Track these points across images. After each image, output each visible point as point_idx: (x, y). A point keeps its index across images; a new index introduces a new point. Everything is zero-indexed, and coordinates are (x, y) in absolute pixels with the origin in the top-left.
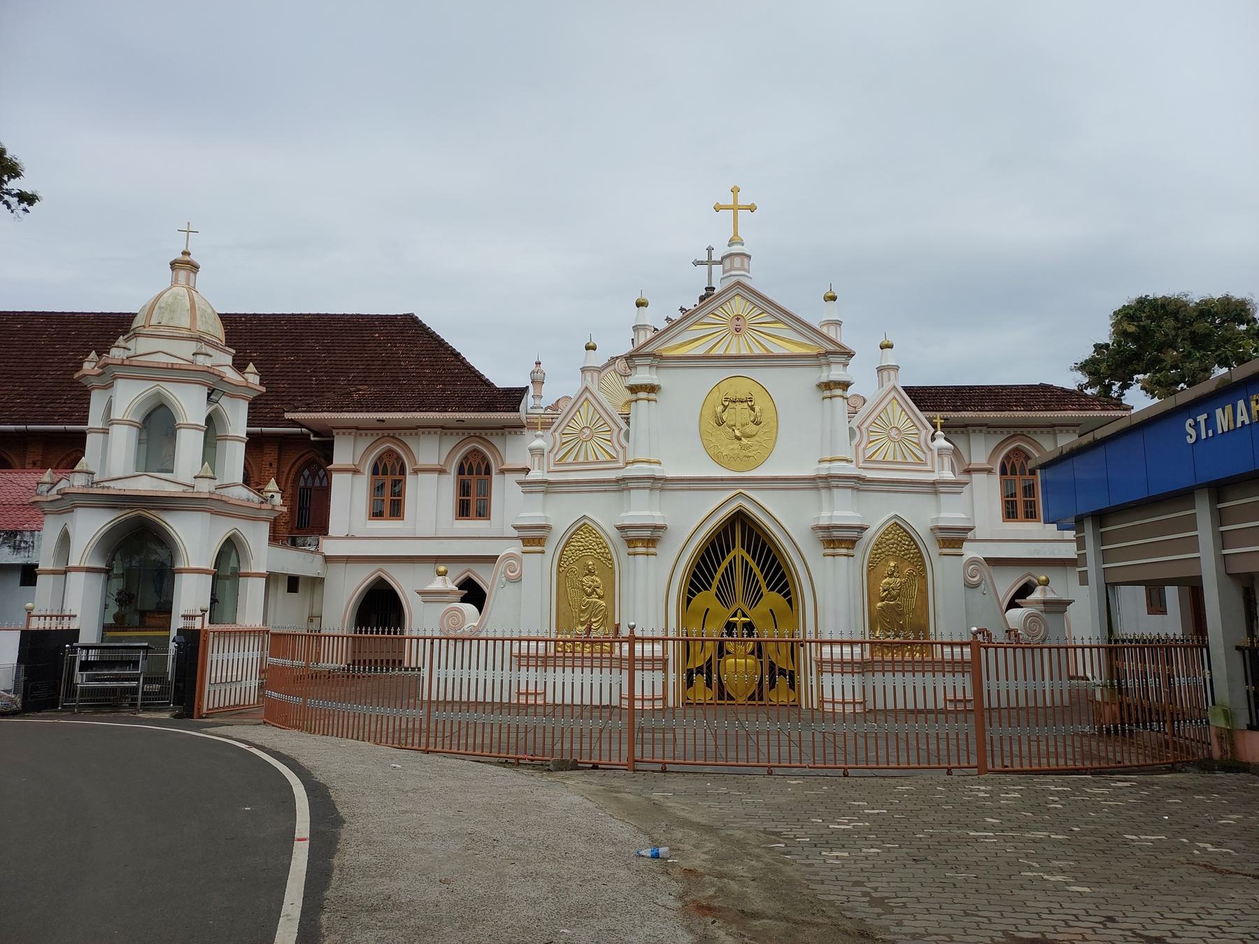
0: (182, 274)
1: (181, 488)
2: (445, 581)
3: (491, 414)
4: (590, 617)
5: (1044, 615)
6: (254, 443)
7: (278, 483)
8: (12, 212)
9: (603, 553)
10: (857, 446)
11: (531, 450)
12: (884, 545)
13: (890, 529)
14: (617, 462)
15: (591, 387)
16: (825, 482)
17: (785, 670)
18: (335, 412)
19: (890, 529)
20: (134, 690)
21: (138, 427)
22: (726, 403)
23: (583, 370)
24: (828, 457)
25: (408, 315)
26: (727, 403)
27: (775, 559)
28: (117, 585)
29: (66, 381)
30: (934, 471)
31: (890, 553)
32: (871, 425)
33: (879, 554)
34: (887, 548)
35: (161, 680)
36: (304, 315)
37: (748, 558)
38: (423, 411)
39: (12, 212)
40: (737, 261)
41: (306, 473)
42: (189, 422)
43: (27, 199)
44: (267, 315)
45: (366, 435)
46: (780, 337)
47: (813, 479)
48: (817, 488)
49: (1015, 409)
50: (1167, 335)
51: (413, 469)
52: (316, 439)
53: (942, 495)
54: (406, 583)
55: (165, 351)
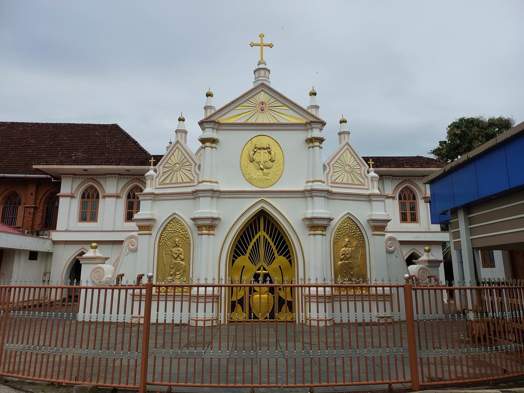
2: (95, 252)
4: (176, 272)
5: (428, 268)
9: (184, 234)
10: (328, 174)
12: (342, 229)
13: (345, 221)
14: (194, 182)
15: (180, 141)
18: (60, 165)
19: (345, 221)
22: (255, 150)
24: (311, 180)
25: (114, 124)
27: (282, 237)
30: (369, 189)
31: (345, 234)
32: (335, 163)
33: (339, 234)
34: (344, 231)
36: (62, 124)
37: (267, 237)
38: (107, 165)
40: (262, 73)
44: (43, 123)
46: (285, 114)
49: (406, 166)
50: (474, 134)
51: (103, 196)
52: (55, 181)
53: (373, 202)
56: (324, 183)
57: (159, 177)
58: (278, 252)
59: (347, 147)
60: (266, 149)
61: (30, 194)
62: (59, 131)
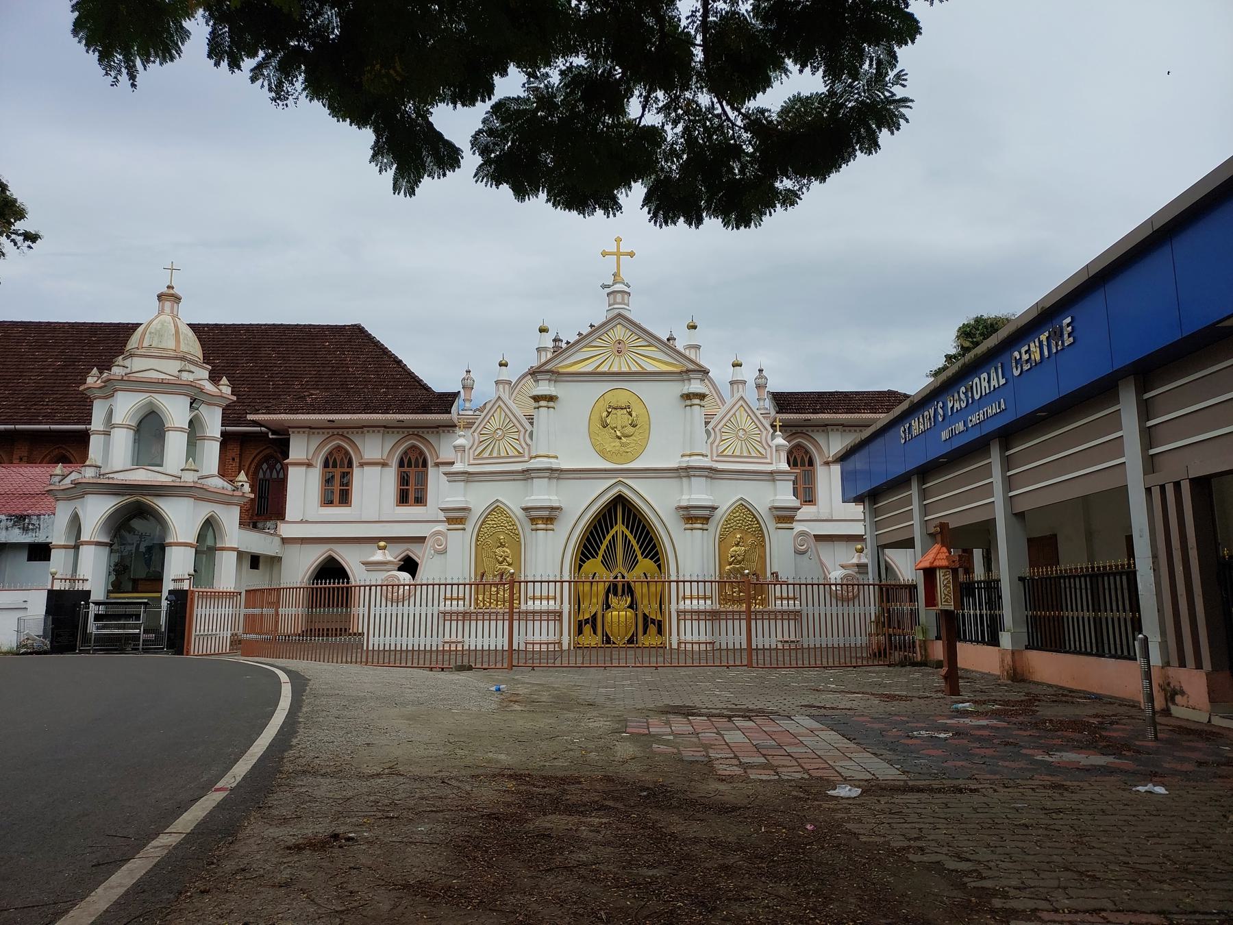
0: (168, 305)
1: (170, 479)
2: (384, 554)
3: (427, 415)
6: (227, 439)
7: (247, 475)
8: (18, 248)
10: (712, 443)
11: (455, 447)
13: (737, 509)
14: (524, 456)
15: (502, 396)
16: (685, 472)
17: (654, 620)
18: (291, 414)
19: (737, 509)
20: (136, 637)
21: (134, 430)
23: (497, 383)
24: (688, 453)
25: (356, 325)
26: (610, 410)
27: (648, 533)
28: (116, 558)
29: (46, 385)
30: (772, 464)
35: (156, 630)
37: (628, 533)
38: (368, 413)
39: (18, 248)
41: (265, 466)
42: (176, 426)
43: (31, 237)
45: (318, 433)
47: (677, 470)
48: (680, 477)
51: (359, 463)
52: (274, 437)
53: (777, 482)
54: (351, 560)
55: (155, 368)
56: (707, 456)
57: (474, 447)
58: (642, 554)
59: (741, 402)
60: (625, 408)
61: (231, 458)
62: (260, 340)
